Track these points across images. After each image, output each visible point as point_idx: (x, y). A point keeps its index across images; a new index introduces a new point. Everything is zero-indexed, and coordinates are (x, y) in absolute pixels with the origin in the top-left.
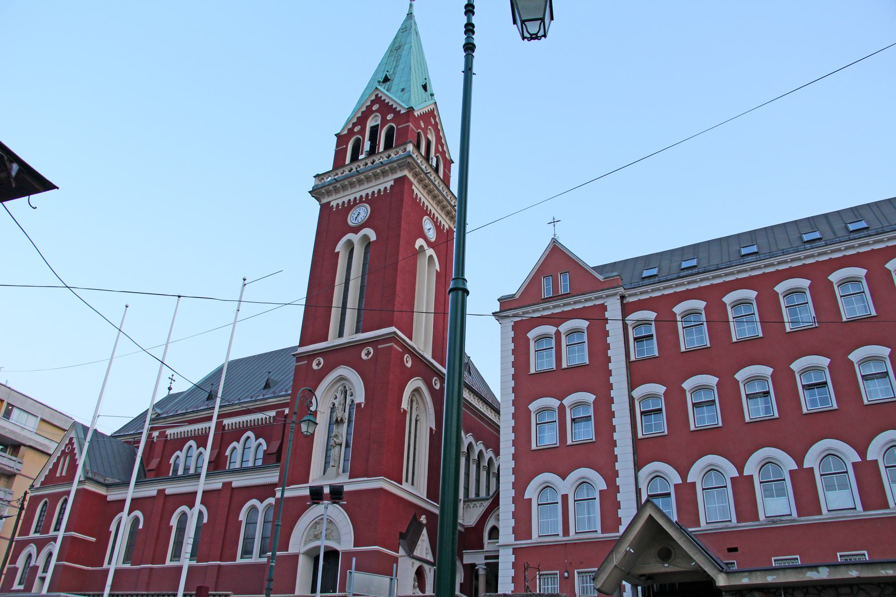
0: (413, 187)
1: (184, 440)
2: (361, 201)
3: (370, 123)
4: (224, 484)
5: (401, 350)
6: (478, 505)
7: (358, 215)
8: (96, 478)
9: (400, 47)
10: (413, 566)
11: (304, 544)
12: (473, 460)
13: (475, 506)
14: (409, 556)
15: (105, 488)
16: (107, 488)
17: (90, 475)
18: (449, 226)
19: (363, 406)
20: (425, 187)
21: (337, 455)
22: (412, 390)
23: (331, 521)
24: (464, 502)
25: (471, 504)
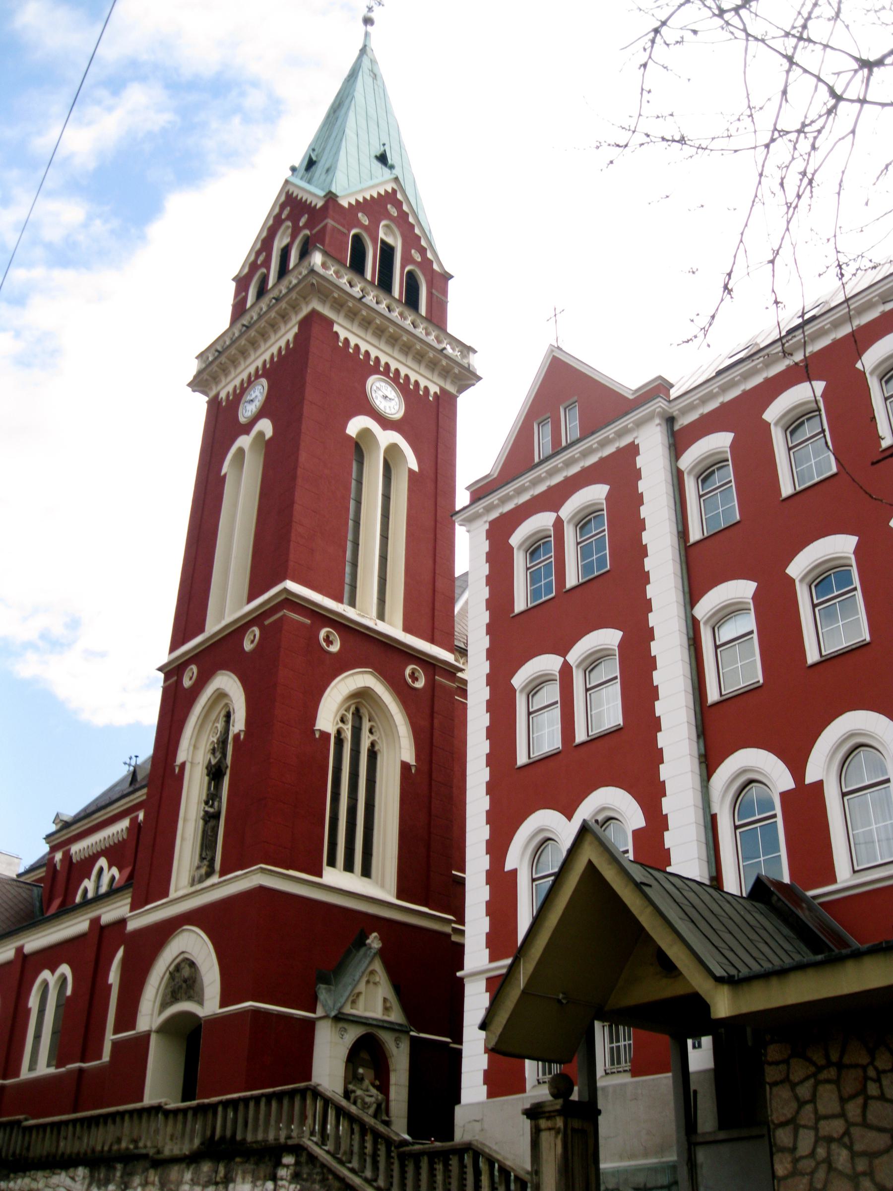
0: (336, 328)
1: (93, 859)
2: (257, 376)
3: (278, 244)
5: (309, 622)
19: (242, 737)
20: (366, 324)
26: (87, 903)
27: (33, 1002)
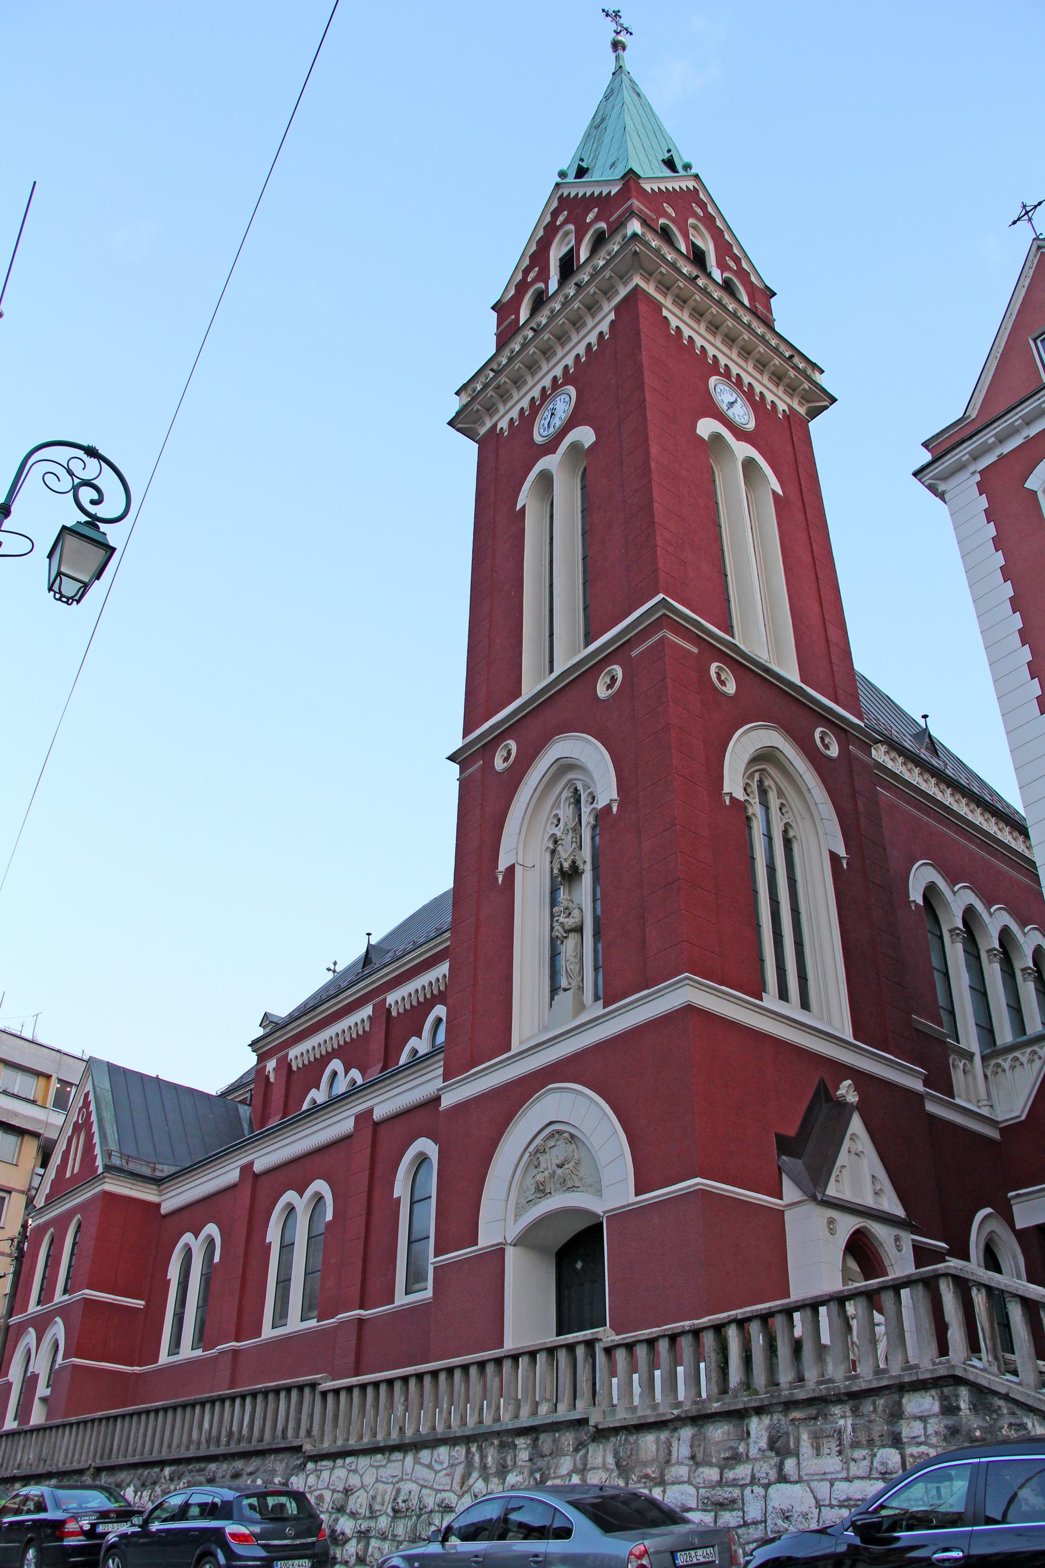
1: (323, 1061)
3: (556, 254)
4: (358, 1118)
6: (1024, 1059)
7: (553, 414)
8: (132, 1166)
9: (603, 120)
10: (832, 1232)
11: (516, 1215)
12: (988, 951)
13: (1017, 1064)
14: (813, 1198)
15: (155, 1187)
16: (159, 1186)
17: (116, 1161)
18: (789, 406)
19: (615, 809)
21: (572, 959)
22: (746, 758)
23: (572, 1136)
24: (984, 1058)
25: (1005, 1060)
26: (317, 1109)
27: (273, 1235)
